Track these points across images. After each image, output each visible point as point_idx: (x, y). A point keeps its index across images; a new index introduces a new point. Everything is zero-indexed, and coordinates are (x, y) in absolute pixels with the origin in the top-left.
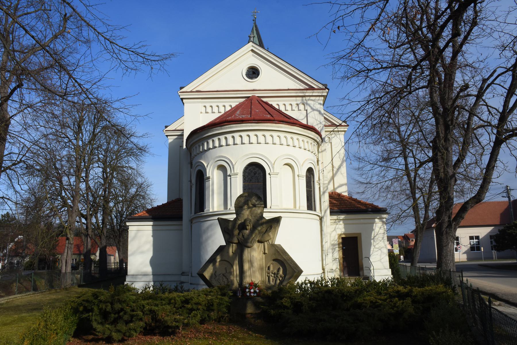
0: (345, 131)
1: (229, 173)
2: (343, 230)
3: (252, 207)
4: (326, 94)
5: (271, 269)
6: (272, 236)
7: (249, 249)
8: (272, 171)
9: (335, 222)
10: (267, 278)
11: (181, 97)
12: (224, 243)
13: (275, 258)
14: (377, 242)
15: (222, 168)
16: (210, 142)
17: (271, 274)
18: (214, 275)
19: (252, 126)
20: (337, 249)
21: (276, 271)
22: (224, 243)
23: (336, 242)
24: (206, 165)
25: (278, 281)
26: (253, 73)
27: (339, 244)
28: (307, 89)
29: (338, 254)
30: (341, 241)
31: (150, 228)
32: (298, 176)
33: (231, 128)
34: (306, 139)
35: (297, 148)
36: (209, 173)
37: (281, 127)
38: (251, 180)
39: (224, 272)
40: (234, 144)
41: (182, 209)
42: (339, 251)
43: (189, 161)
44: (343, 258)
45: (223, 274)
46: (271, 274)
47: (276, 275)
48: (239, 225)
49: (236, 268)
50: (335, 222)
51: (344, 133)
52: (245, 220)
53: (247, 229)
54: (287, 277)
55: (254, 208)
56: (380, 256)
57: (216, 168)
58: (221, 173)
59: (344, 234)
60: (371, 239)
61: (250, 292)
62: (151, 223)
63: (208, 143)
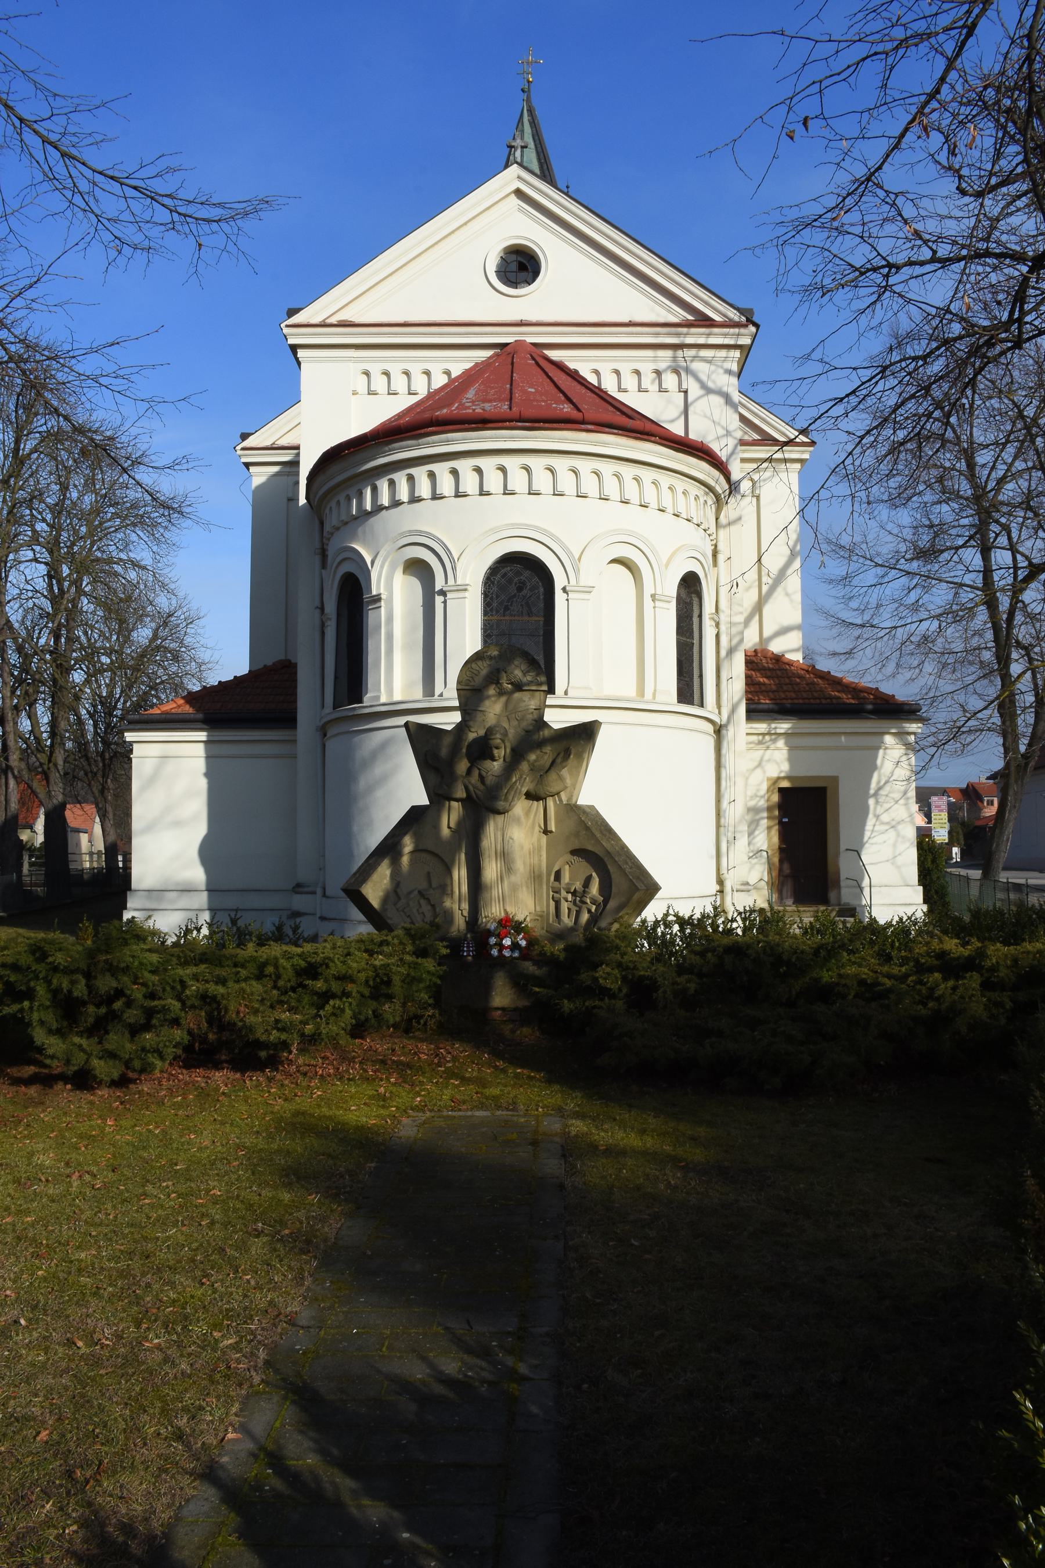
0: (801, 461)
1: (439, 584)
2: (785, 767)
3: (512, 692)
4: (746, 341)
5: (566, 878)
6: (569, 782)
7: (500, 819)
8: (573, 581)
9: (760, 743)
10: (552, 904)
13: (576, 846)
14: (887, 806)
15: (418, 568)
16: (383, 485)
17: (564, 893)
18: (393, 895)
19: (512, 438)
20: (764, 823)
21: (578, 885)
23: (763, 803)
24: (368, 559)
25: (585, 917)
26: (520, 266)
27: (769, 809)
28: (688, 325)
29: (765, 838)
30: (775, 798)
31: (200, 750)
33: (448, 442)
35: (652, 513)
36: (377, 585)
37: (605, 444)
38: (506, 608)
39: (423, 885)
42: (769, 828)
43: (318, 545)
45: (420, 892)
46: (564, 893)
47: (579, 896)
48: (471, 745)
49: (460, 875)
50: (760, 743)
51: (798, 466)
52: (490, 731)
53: (493, 759)
54: (612, 904)
55: (517, 695)
56: (895, 845)
58: (416, 585)
59: (788, 778)
60: (866, 796)
61: (501, 947)
62: (202, 736)
63: (375, 489)
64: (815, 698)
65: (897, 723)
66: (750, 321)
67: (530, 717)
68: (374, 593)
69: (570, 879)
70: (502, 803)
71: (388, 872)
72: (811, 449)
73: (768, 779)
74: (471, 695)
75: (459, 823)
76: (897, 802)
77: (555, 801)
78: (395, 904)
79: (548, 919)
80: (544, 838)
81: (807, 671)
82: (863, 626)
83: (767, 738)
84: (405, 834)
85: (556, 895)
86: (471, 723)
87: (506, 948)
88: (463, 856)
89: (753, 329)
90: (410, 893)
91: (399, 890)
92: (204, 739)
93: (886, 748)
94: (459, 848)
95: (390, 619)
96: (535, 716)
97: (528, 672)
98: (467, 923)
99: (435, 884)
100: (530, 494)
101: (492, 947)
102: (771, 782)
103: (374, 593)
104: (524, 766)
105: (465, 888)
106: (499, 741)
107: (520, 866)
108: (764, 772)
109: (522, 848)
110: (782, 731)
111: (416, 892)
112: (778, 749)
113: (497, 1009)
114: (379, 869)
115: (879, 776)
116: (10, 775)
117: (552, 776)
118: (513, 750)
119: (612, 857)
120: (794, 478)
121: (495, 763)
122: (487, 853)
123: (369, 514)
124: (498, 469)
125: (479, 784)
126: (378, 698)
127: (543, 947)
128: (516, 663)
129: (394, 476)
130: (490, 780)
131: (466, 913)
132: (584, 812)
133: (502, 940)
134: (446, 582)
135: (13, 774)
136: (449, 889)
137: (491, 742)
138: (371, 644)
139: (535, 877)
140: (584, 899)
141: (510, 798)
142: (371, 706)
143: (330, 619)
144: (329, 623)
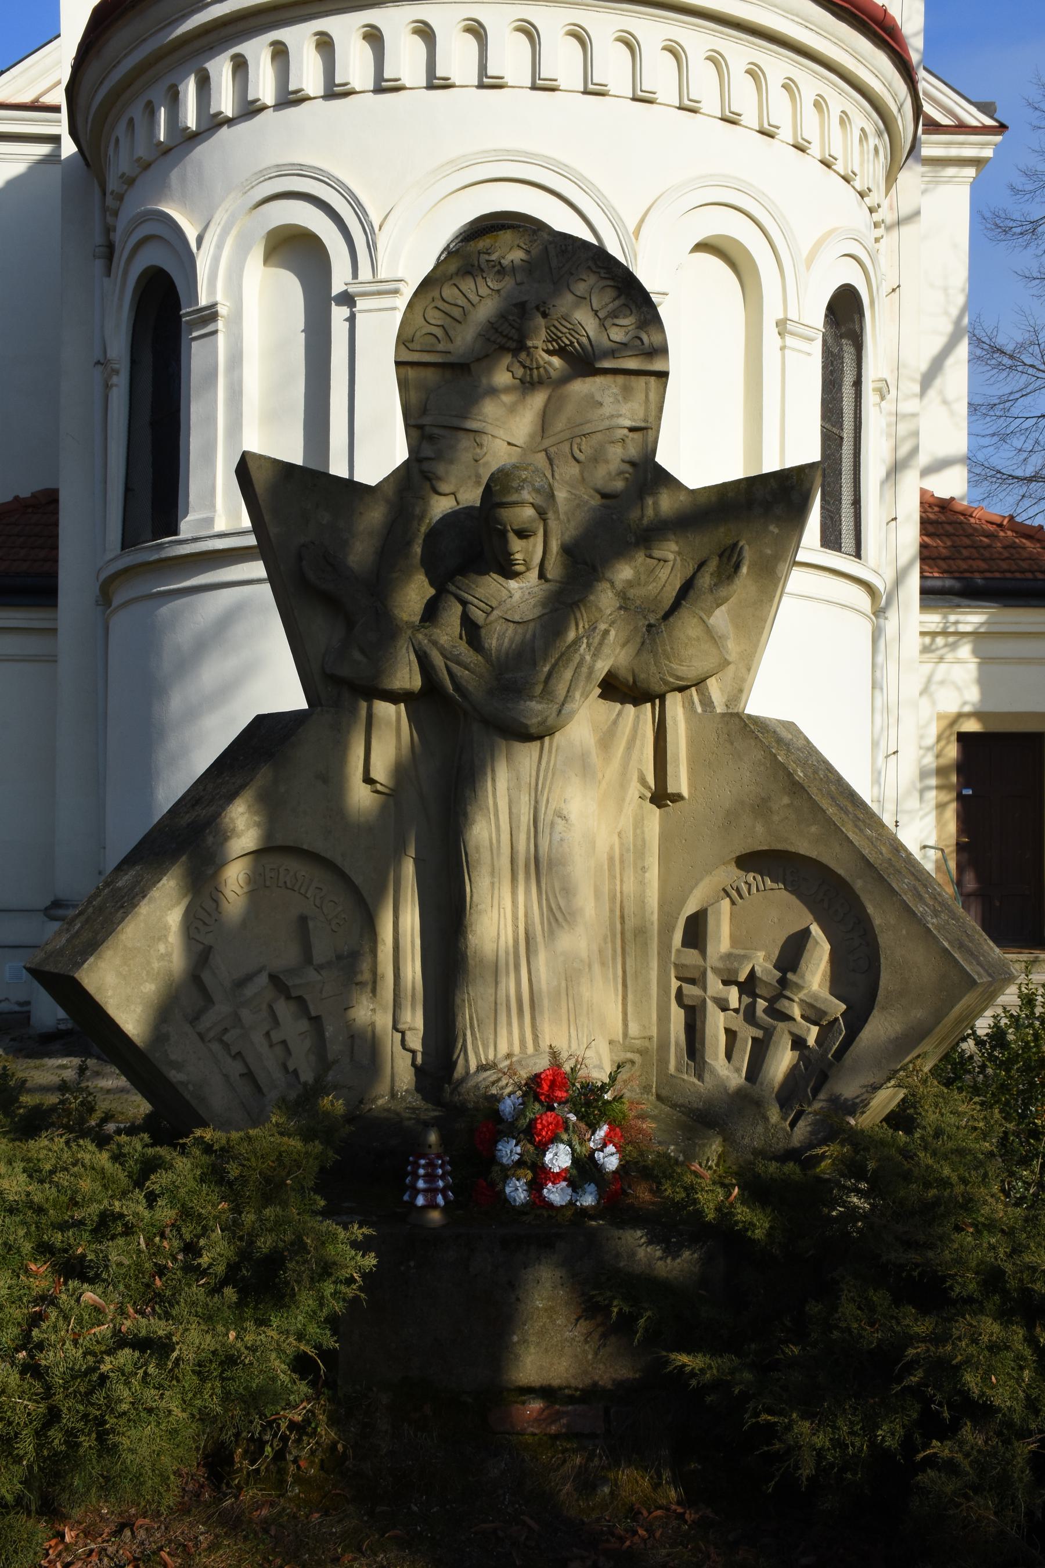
0: (977, 162)
1: (340, 281)
3: (565, 380)
5: (721, 938)
6: (733, 648)
7: (527, 754)
10: (677, 1016)
12: (282, 690)
13: (757, 837)
15: (296, 251)
16: (221, 69)
17: (714, 985)
18: (188, 1000)
21: (762, 962)
22: (282, 690)
24: (191, 234)
25: (783, 1061)
30: (952, 752)
32: (782, 327)
34: (841, 100)
35: (780, 149)
36: (210, 286)
39: (287, 955)
40: (379, 90)
41: (55, 536)
42: (941, 807)
43: (99, 239)
44: (960, 847)
45: (274, 978)
46: (714, 985)
47: (766, 998)
48: (435, 533)
49: (402, 926)
51: (971, 172)
52: (498, 489)
53: (508, 571)
54: (879, 1029)
55: (581, 387)
57: (257, 253)
58: (289, 286)
59: (977, 715)
61: (541, 1175)
63: (204, 83)
64: (1022, 572)
67: (616, 454)
68: (203, 301)
69: (734, 940)
70: (534, 705)
71: (174, 918)
72: (998, 139)
73: (940, 717)
74: (440, 391)
75: (400, 772)
77: (689, 706)
78: (194, 1020)
79: (663, 1061)
80: (654, 814)
81: (1000, 525)
82: (1030, 479)
83: (940, 641)
84: (231, 797)
85: (689, 990)
86: (440, 469)
87: (556, 1178)
88: (409, 869)
90: (241, 983)
91: (206, 976)
94: (399, 852)
95: (236, 360)
96: (633, 451)
97: (614, 314)
98: (419, 1071)
99: (321, 951)
100: (534, 87)
101: (507, 1173)
102: (945, 723)
103: (203, 301)
104: (605, 599)
105: (413, 970)
106: (529, 512)
107: (589, 906)
108: (934, 703)
109: (593, 844)
110: (969, 628)
111: (263, 980)
112: (959, 661)
113: (529, 1391)
114: (144, 909)
117: (687, 627)
118: (567, 550)
119: (882, 879)
120: (963, 194)
121: (513, 584)
122: (485, 856)
124: (468, 30)
125: (463, 649)
126: (210, 521)
127: (690, 1189)
128: (581, 288)
129: (242, 48)
130: (499, 637)
131: (416, 1042)
132: (779, 740)
133: (542, 1149)
134: (355, 275)
136: (365, 966)
137: (506, 514)
138: (196, 411)
139: (627, 936)
140: (783, 1005)
141: (561, 689)
142: (195, 540)
143: (117, 372)
144: (115, 379)
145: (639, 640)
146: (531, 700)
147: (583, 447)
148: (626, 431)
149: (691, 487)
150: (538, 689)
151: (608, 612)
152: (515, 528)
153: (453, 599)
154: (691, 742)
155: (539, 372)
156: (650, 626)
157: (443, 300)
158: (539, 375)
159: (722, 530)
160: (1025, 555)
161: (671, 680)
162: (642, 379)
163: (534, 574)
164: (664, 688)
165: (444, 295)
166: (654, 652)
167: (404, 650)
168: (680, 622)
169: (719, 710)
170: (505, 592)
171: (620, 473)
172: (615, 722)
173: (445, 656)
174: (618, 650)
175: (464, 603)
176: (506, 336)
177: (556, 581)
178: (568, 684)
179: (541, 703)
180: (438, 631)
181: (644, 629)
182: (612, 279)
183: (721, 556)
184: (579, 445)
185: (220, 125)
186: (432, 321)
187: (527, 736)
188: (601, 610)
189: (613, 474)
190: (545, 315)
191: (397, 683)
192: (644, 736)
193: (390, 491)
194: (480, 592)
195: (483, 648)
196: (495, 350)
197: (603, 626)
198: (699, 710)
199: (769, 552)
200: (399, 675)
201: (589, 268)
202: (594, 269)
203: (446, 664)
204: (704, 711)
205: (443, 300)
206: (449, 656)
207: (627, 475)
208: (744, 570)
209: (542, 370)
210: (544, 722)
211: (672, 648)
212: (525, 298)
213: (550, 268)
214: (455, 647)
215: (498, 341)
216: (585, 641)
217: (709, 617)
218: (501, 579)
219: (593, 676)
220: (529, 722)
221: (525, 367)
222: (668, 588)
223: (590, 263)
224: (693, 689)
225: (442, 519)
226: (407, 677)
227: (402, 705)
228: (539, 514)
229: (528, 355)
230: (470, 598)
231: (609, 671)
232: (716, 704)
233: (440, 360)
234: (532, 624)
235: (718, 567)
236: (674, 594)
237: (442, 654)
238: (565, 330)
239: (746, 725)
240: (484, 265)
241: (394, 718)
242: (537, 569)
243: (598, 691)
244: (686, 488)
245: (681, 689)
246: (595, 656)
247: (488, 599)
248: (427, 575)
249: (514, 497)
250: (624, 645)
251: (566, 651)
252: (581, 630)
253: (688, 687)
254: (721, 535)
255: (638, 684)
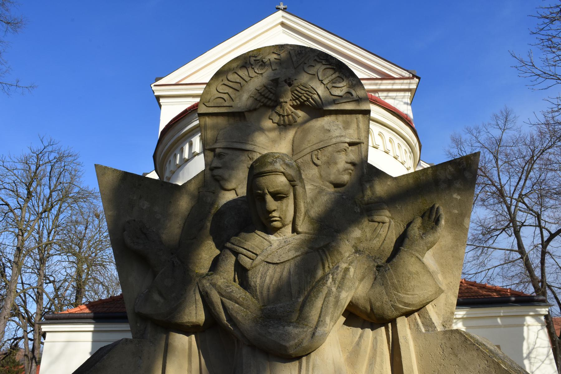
4: (414, 86)
11: (156, 94)
31: (89, 337)
34: (397, 140)
53: (272, 230)
62: (91, 327)
63: (191, 145)
65: (532, 308)
66: (414, 76)
67: (342, 161)
76: (543, 362)
77: (415, 327)
89: (417, 80)
92: (92, 329)
93: (528, 326)
106: (282, 180)
110: (460, 317)
115: (528, 344)
116: (34, 361)
117: (408, 262)
121: (272, 238)
123: (187, 161)
130: (265, 277)
135: (35, 360)
145: (372, 277)
146: (289, 326)
147: (319, 156)
148: (347, 145)
149: (394, 176)
150: (295, 317)
151: (347, 254)
152: (271, 190)
153: (228, 252)
154: (421, 356)
155: (288, 118)
156: (378, 267)
157: (228, 80)
158: (289, 120)
159: (420, 200)
160: (472, 291)
161: (401, 306)
162: (354, 117)
163: (289, 228)
164: (395, 313)
165: (229, 78)
166: (384, 284)
167: (192, 292)
168: (402, 261)
169: (439, 330)
170: (266, 243)
171: (346, 170)
172: (358, 344)
173: (221, 294)
174: (357, 284)
175: (236, 254)
176: (267, 98)
177: (306, 233)
178: (319, 310)
179: (297, 327)
180: (218, 276)
181: (375, 269)
182: (330, 65)
183: (422, 217)
184: (317, 155)
185: (195, 156)
186: (221, 91)
187: (288, 358)
188: (341, 254)
189: (341, 170)
190: (290, 85)
191: (186, 317)
192: (382, 353)
193: (192, 188)
194: (249, 245)
195: (250, 286)
196: (261, 106)
197: (344, 265)
198: (423, 330)
199: (456, 212)
200: (187, 311)
201: (315, 60)
202: (318, 60)
203: (221, 300)
204: (427, 331)
205: (228, 80)
206: (224, 294)
207: (351, 171)
208: (443, 222)
209: (290, 117)
210: (299, 344)
211: (398, 281)
212: (277, 77)
213: (292, 61)
214: (228, 286)
215: (262, 100)
216: (331, 276)
217: (423, 257)
218: (263, 234)
219: (339, 304)
220: (287, 345)
221: (279, 115)
222: (387, 241)
223: (316, 58)
224: (416, 314)
225: (225, 204)
226: (196, 314)
227: (193, 336)
228: (290, 181)
229: (281, 108)
230: (241, 250)
231: (351, 302)
232: (436, 324)
233: (226, 111)
234: (287, 265)
235: (422, 223)
236: (393, 245)
237: (219, 292)
238: (303, 92)
239: (466, 339)
240: (252, 62)
241: (187, 347)
242: (291, 225)
243: (343, 319)
244: (391, 177)
245: (408, 314)
246: (340, 288)
247: (254, 248)
248: (214, 241)
249: (270, 168)
250: (361, 280)
251: (315, 285)
252: (327, 270)
253: (412, 312)
254: (422, 204)
255: (375, 311)
